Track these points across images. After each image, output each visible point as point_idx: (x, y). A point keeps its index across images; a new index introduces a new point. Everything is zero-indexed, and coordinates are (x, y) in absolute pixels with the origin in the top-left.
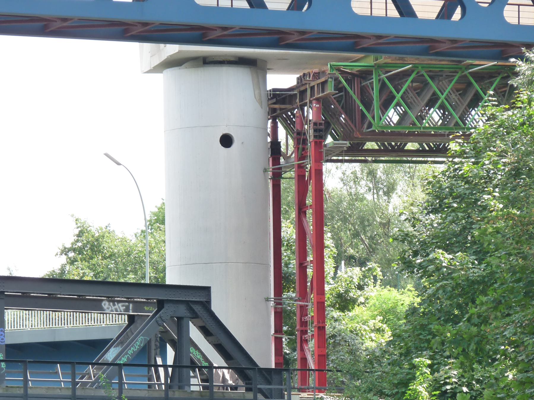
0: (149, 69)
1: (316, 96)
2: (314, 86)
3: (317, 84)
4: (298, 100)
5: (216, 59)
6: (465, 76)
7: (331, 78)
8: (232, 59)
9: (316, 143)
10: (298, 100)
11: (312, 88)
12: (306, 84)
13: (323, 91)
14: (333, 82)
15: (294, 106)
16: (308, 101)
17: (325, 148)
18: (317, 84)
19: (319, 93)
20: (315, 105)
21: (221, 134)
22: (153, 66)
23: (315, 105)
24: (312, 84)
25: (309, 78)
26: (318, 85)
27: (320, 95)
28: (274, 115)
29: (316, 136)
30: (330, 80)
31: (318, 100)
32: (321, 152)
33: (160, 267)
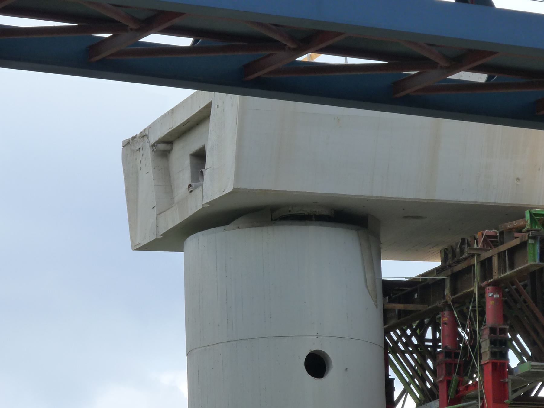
0: (153, 238)
1: (496, 276)
2: (490, 259)
3: (499, 254)
4: (447, 292)
5: (295, 211)
6: (454, 301)
7: (534, 238)
8: (325, 212)
9: (494, 365)
10: (447, 292)
11: (486, 264)
12: (473, 255)
13: (512, 267)
14: (538, 246)
15: (439, 304)
16: (475, 289)
17: (510, 377)
18: (499, 254)
19: (502, 269)
20: (490, 294)
21: (330, 356)
22: (163, 231)
23: (490, 294)
24: (485, 255)
25: (477, 246)
26: (501, 255)
27: (508, 273)
28: (390, 320)
29: (495, 352)
30: (531, 241)
31: (497, 285)
32: (505, 384)
33: (162, 146)
